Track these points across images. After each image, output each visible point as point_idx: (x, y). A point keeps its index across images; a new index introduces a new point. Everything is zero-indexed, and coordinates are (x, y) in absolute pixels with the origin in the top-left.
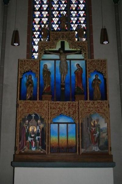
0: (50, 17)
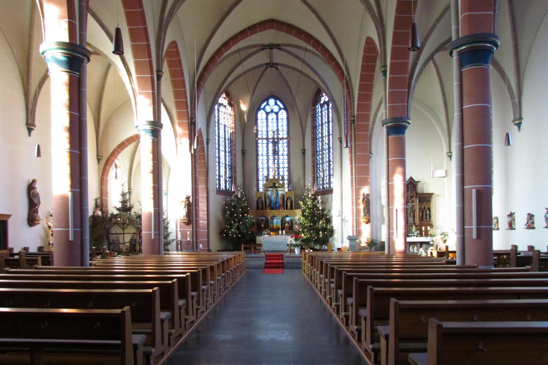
0: (268, 171)
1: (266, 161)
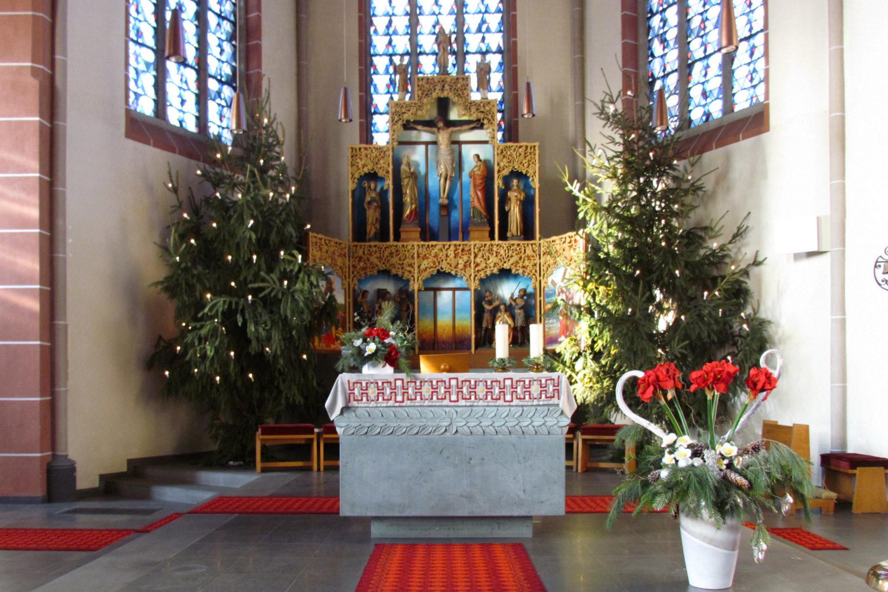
1: (406, 20)
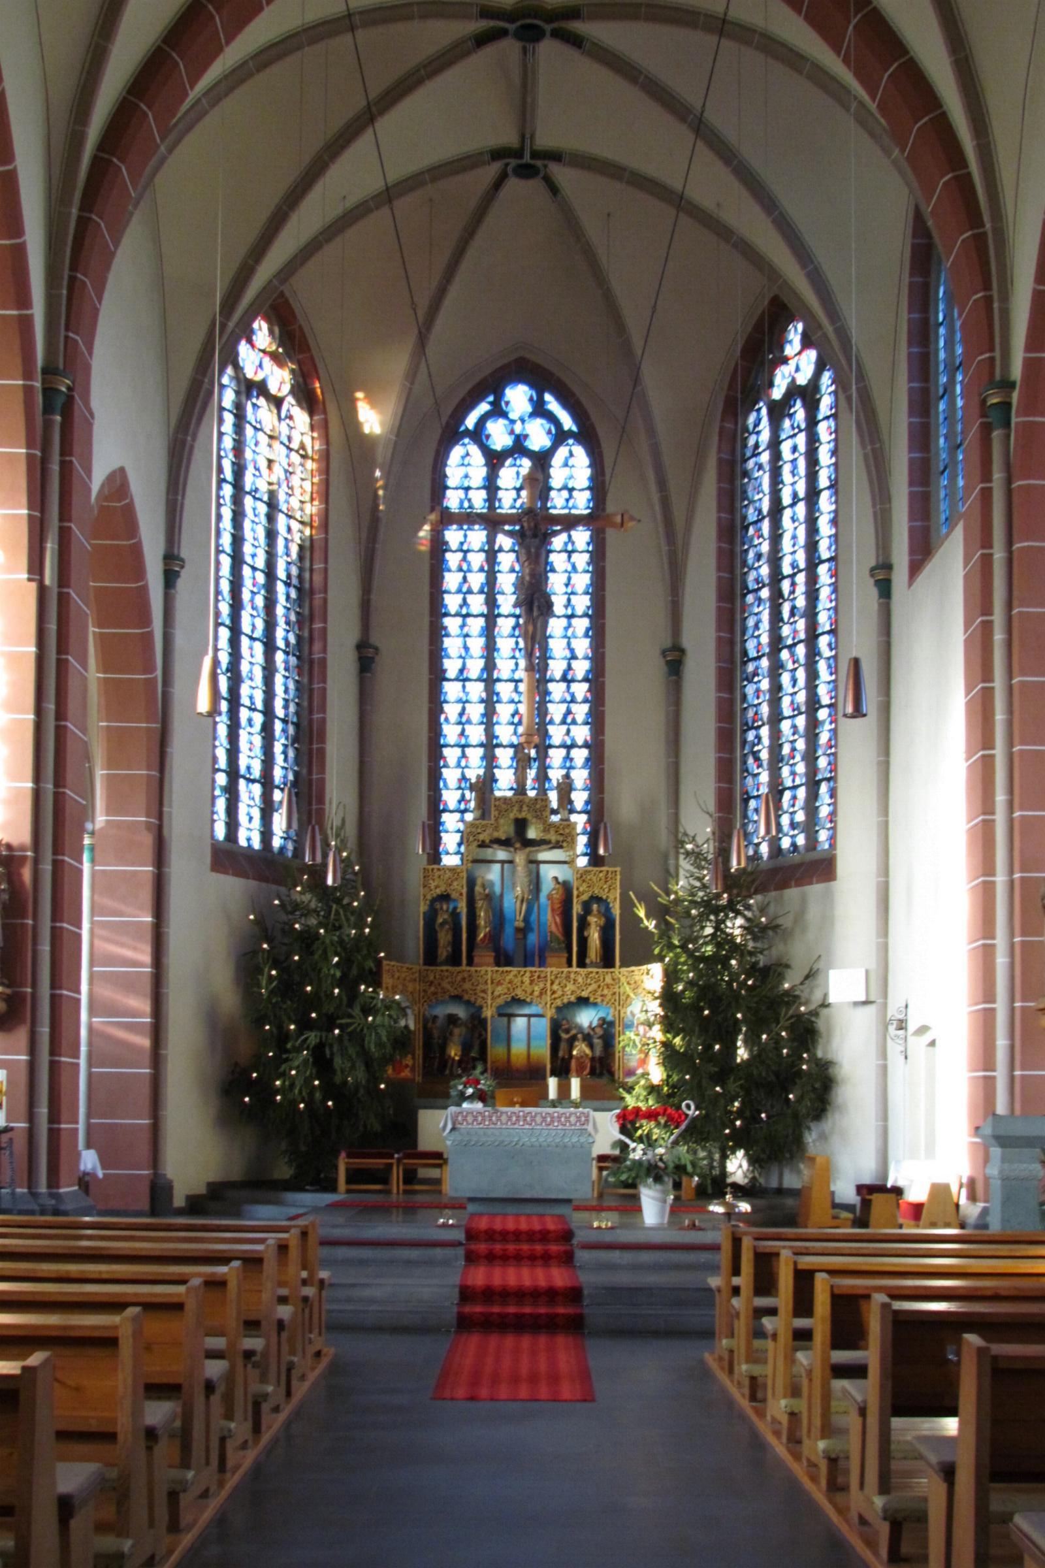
0: (490, 759)
1: (481, 708)
